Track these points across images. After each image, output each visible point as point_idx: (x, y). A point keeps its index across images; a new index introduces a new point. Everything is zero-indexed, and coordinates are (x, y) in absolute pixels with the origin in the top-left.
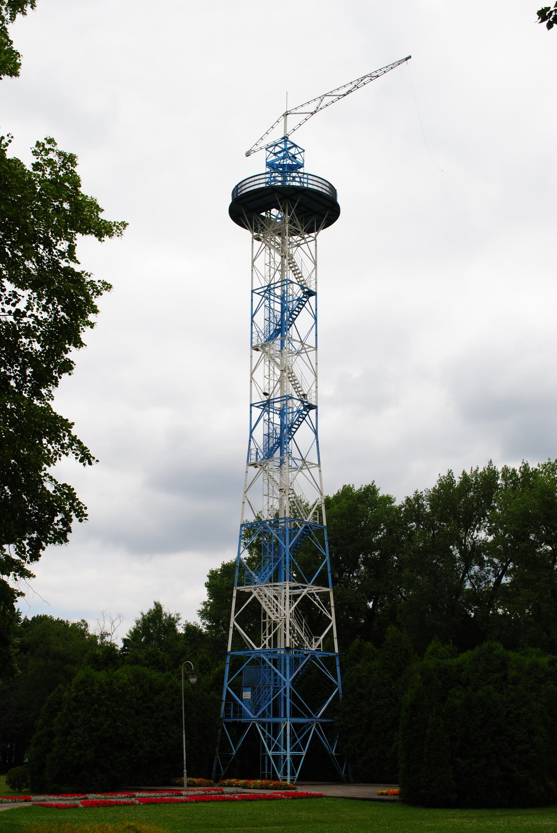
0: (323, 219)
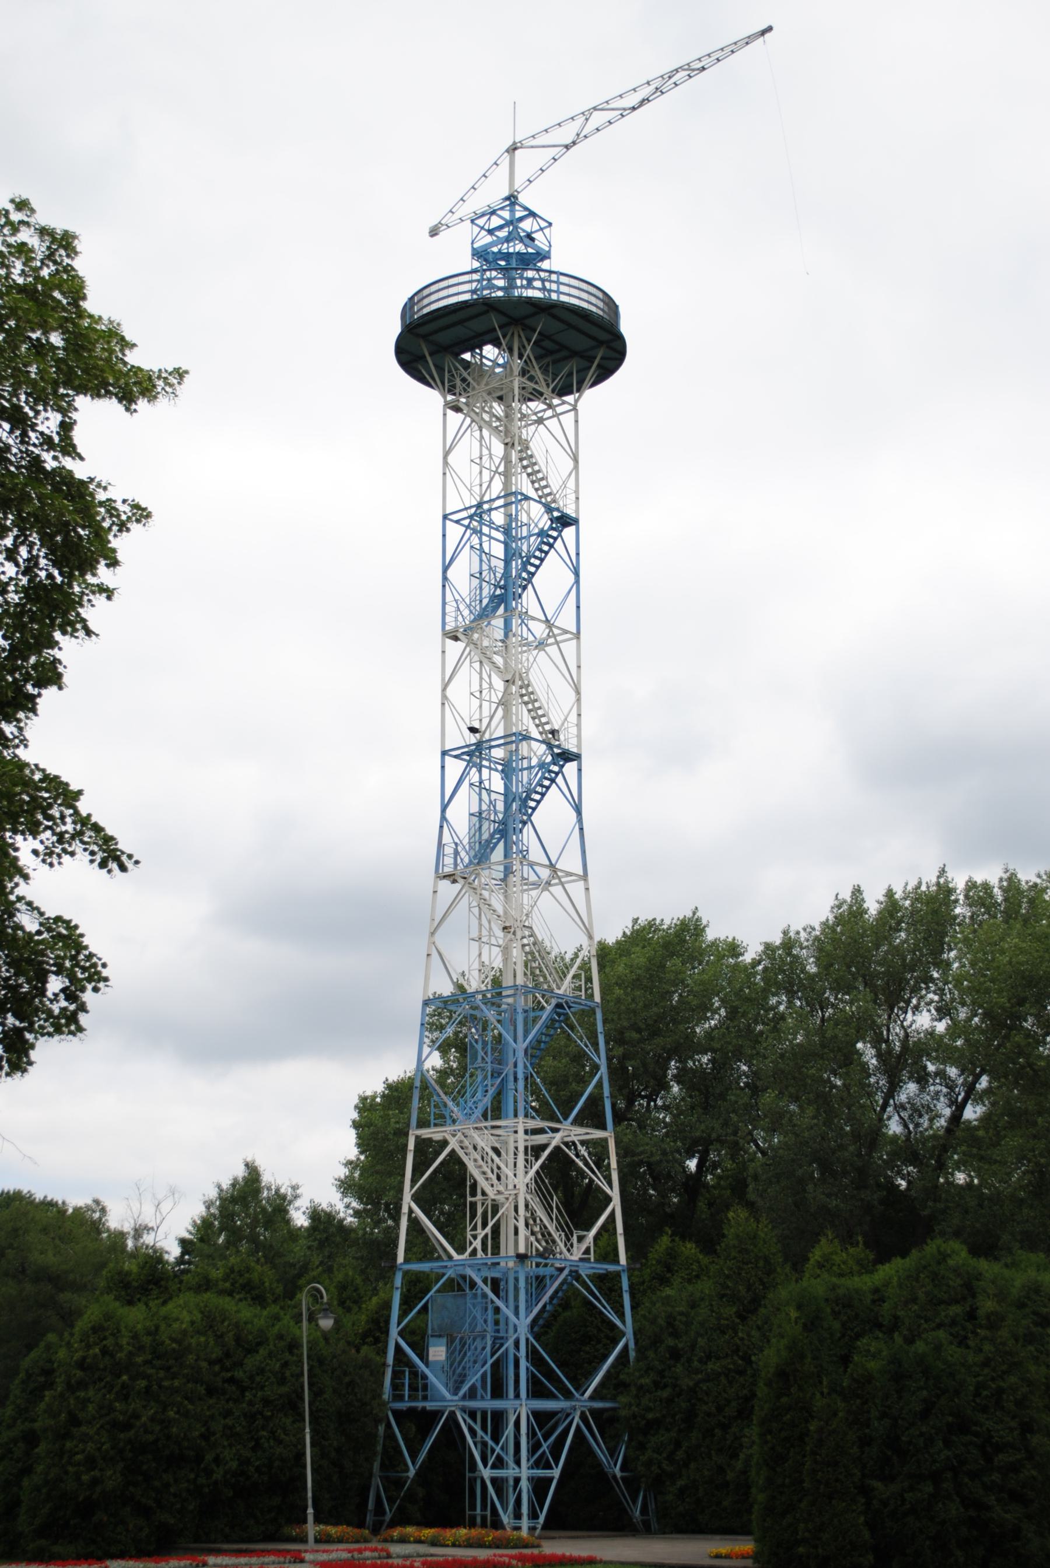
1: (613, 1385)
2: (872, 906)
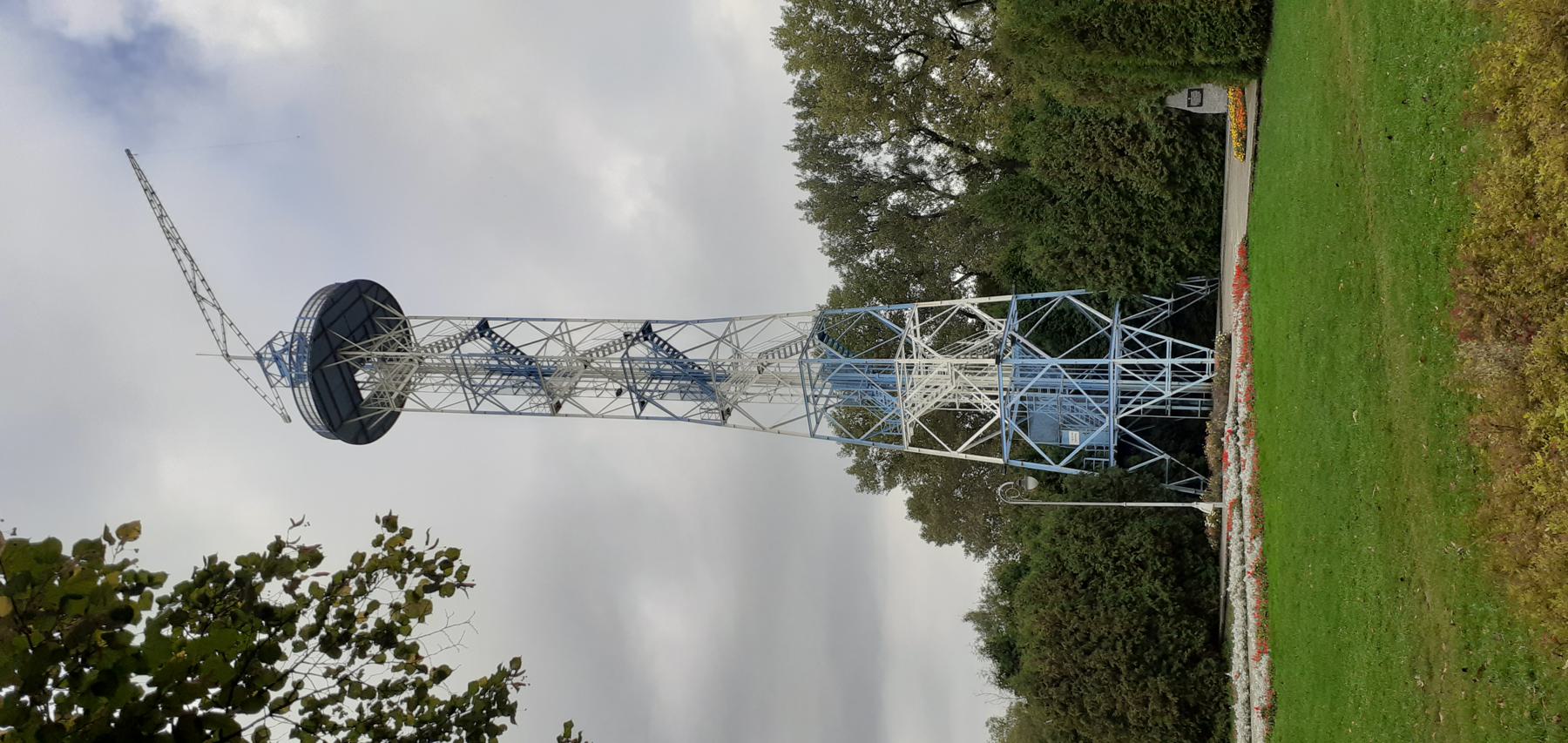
0: (383, 309)
1: (1104, 303)
2: (806, 195)
